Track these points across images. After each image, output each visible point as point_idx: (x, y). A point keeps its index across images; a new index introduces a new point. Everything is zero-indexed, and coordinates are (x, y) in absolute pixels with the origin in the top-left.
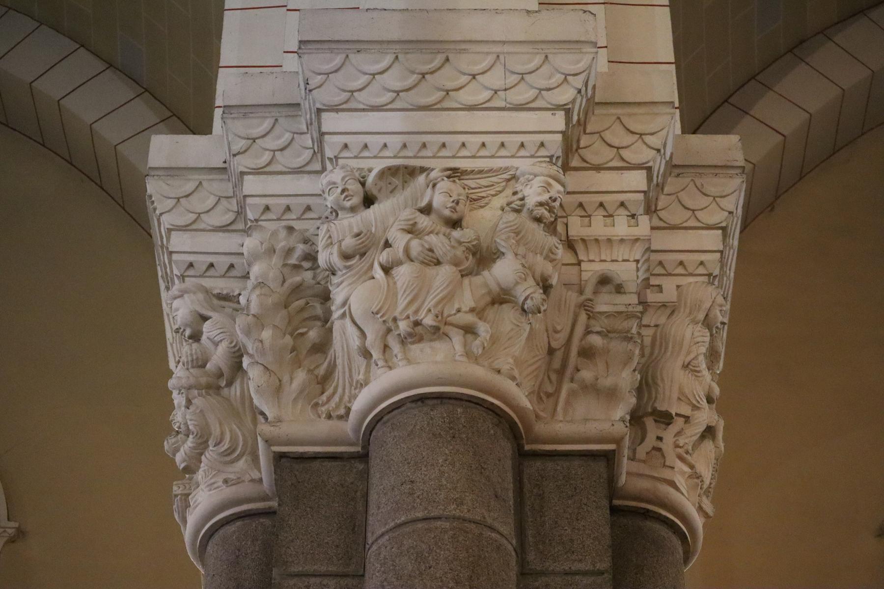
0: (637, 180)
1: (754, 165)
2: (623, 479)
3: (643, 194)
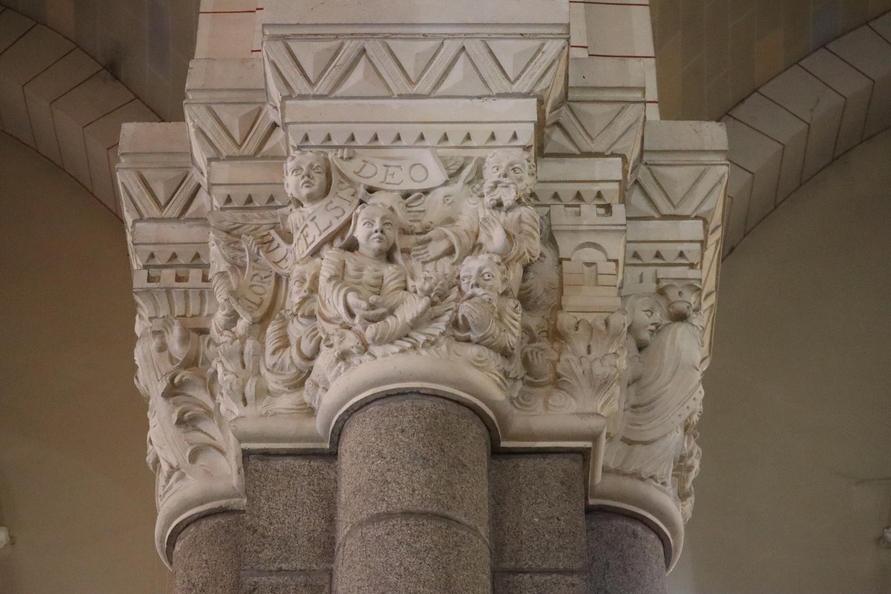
0: (612, 169)
1: (783, 145)
2: (598, 477)
3: (618, 183)
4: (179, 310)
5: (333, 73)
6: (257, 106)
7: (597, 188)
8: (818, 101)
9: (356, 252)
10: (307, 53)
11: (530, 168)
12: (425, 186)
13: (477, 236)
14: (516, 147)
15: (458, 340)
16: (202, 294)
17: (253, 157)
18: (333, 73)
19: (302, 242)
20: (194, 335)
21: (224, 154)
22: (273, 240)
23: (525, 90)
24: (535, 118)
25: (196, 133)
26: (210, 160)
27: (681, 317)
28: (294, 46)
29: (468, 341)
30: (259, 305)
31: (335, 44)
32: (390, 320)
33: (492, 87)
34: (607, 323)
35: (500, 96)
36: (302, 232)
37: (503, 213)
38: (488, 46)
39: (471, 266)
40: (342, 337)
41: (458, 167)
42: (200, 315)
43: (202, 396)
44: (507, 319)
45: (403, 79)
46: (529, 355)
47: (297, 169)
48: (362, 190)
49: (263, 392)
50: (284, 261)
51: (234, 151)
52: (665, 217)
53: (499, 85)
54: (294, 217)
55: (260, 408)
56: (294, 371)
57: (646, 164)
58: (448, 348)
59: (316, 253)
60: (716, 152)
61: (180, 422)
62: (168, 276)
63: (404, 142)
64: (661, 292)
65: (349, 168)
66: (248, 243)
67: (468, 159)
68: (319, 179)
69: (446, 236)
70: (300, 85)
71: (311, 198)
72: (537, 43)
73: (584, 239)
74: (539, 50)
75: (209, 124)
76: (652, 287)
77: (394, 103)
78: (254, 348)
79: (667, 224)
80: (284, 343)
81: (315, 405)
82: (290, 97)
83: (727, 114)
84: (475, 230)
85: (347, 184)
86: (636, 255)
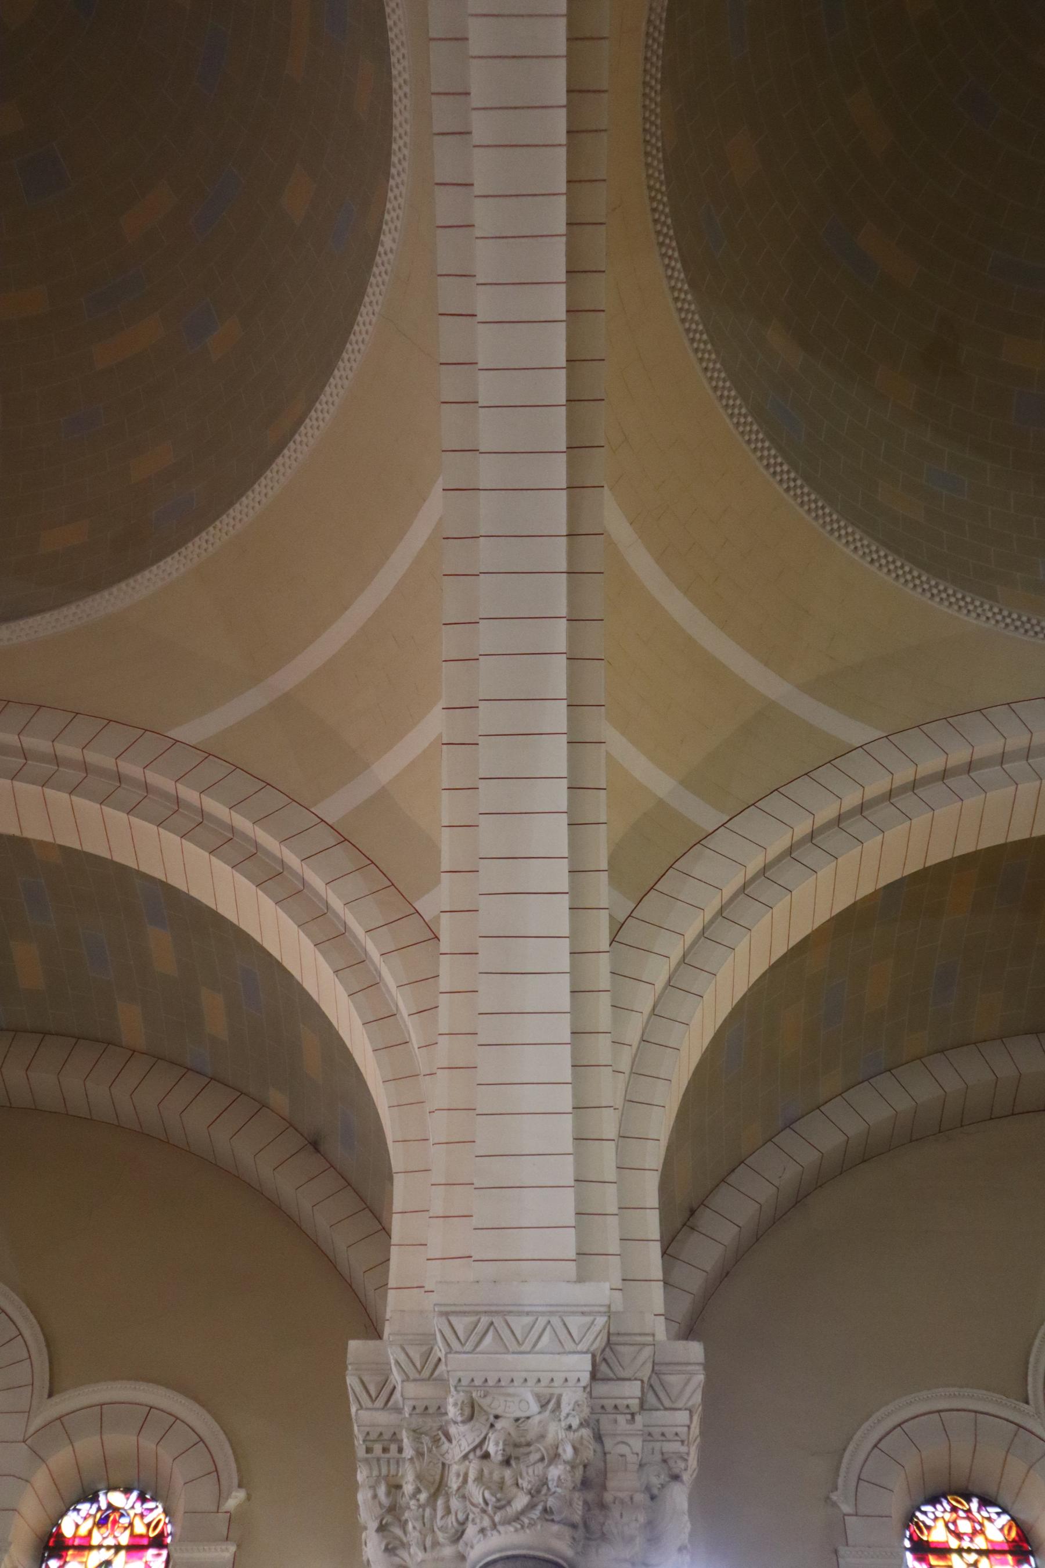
0: (633, 1389)
4: (384, 1471)
5: (474, 1338)
6: (430, 1346)
7: (625, 1402)
8: (785, 1169)
9: (489, 1460)
10: (461, 1324)
11: (587, 1403)
12: (527, 1414)
13: (557, 1448)
14: (579, 1387)
15: (547, 1520)
16: (398, 1463)
17: (429, 1379)
18: (474, 1338)
19: (458, 1447)
20: (393, 1490)
21: (411, 1378)
22: (440, 1439)
23: (584, 1350)
24: (590, 1368)
25: (395, 1364)
26: (403, 1381)
27: (676, 1478)
28: (453, 1319)
29: (553, 1521)
30: (433, 1483)
31: (474, 1319)
32: (508, 1509)
33: (566, 1347)
34: (631, 1498)
35: (570, 1353)
36: (458, 1442)
37: (572, 1433)
38: (563, 1320)
39: (555, 1472)
40: (482, 1519)
41: (546, 1401)
42: (397, 1475)
43: (398, 1531)
44: (575, 1505)
45: (515, 1343)
46: (587, 1520)
47: (455, 1404)
48: (492, 1418)
49: (436, 1544)
50: (447, 1454)
51: (417, 1376)
52: (666, 1409)
53: (569, 1345)
54: (453, 1430)
55: (434, 1554)
56: (453, 1530)
57: (656, 1373)
58: (542, 1526)
59: (465, 1457)
60: (698, 1364)
61: (387, 1549)
62: (378, 1448)
63: (515, 1383)
64: (665, 1461)
65: (484, 1402)
66: (426, 1439)
67: (552, 1395)
68: (467, 1411)
69: (540, 1449)
70: (455, 1345)
71: (463, 1422)
72: (592, 1318)
73: (619, 1439)
74: (593, 1323)
75: (402, 1358)
76: (658, 1457)
77: (509, 1357)
78: (431, 1514)
79: (667, 1413)
80: (448, 1511)
81: (466, 1555)
82: (450, 1353)
83: (723, 1180)
84: (556, 1443)
85: (483, 1413)
86: (650, 1434)
